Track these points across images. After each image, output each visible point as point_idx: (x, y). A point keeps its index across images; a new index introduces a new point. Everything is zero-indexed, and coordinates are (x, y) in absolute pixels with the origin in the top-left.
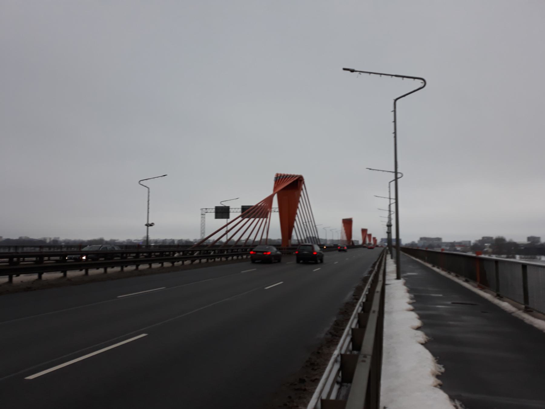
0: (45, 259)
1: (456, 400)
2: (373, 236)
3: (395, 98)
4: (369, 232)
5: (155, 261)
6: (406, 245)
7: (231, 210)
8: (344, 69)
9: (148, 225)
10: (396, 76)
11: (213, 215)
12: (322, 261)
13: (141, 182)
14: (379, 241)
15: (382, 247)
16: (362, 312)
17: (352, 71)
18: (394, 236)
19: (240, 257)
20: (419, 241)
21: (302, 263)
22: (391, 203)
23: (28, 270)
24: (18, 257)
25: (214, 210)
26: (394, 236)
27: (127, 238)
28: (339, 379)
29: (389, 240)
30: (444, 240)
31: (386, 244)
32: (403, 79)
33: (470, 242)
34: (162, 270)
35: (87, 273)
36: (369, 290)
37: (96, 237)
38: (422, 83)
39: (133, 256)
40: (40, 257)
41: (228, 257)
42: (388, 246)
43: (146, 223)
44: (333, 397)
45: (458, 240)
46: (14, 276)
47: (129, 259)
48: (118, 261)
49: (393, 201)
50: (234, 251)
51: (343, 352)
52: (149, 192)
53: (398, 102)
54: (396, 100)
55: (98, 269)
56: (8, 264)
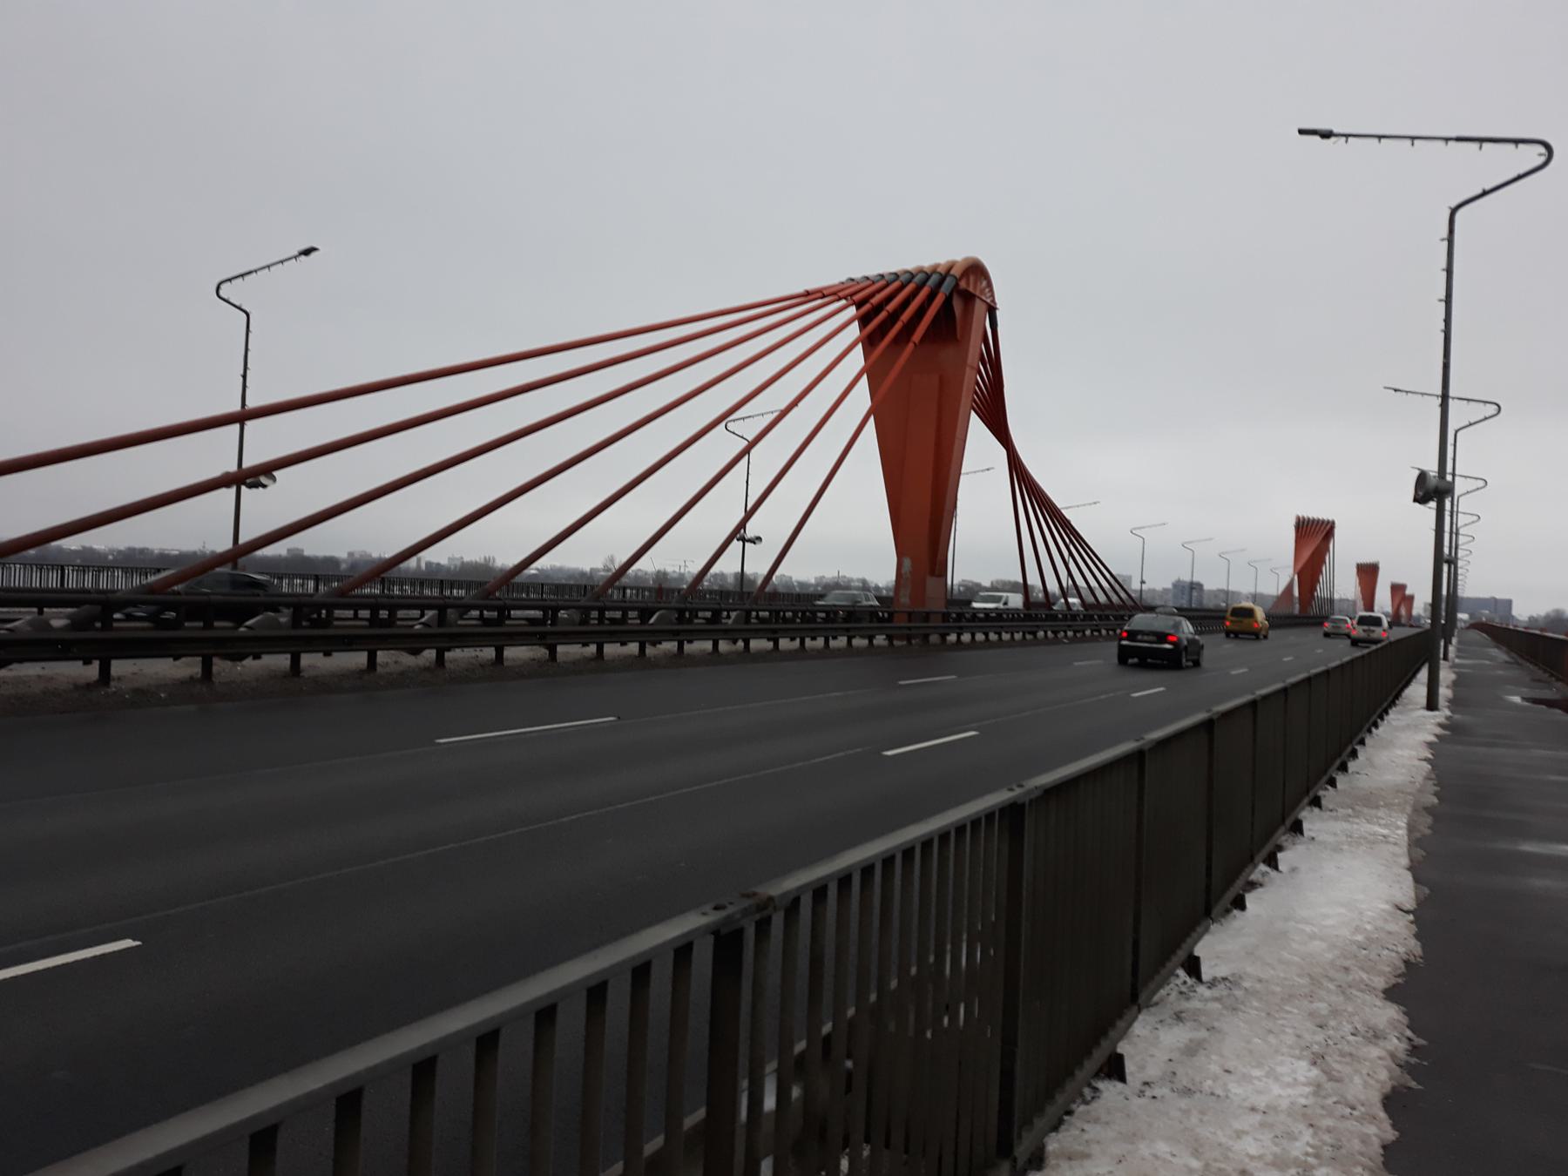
0: (399, 616)
3: (1454, 204)
4: (1408, 592)
5: (758, 634)
8: (1301, 132)
10: (1459, 139)
12: (1197, 664)
17: (1326, 135)
19: (966, 637)
21: (1133, 665)
23: (348, 643)
24: (393, 609)
27: (819, 574)
34: (826, 652)
35: (440, 658)
38: (1540, 155)
39: (704, 618)
40: (551, 611)
41: (948, 634)
47: (631, 624)
48: (636, 628)
54: (1454, 212)
55: (623, 644)
56: (146, 624)
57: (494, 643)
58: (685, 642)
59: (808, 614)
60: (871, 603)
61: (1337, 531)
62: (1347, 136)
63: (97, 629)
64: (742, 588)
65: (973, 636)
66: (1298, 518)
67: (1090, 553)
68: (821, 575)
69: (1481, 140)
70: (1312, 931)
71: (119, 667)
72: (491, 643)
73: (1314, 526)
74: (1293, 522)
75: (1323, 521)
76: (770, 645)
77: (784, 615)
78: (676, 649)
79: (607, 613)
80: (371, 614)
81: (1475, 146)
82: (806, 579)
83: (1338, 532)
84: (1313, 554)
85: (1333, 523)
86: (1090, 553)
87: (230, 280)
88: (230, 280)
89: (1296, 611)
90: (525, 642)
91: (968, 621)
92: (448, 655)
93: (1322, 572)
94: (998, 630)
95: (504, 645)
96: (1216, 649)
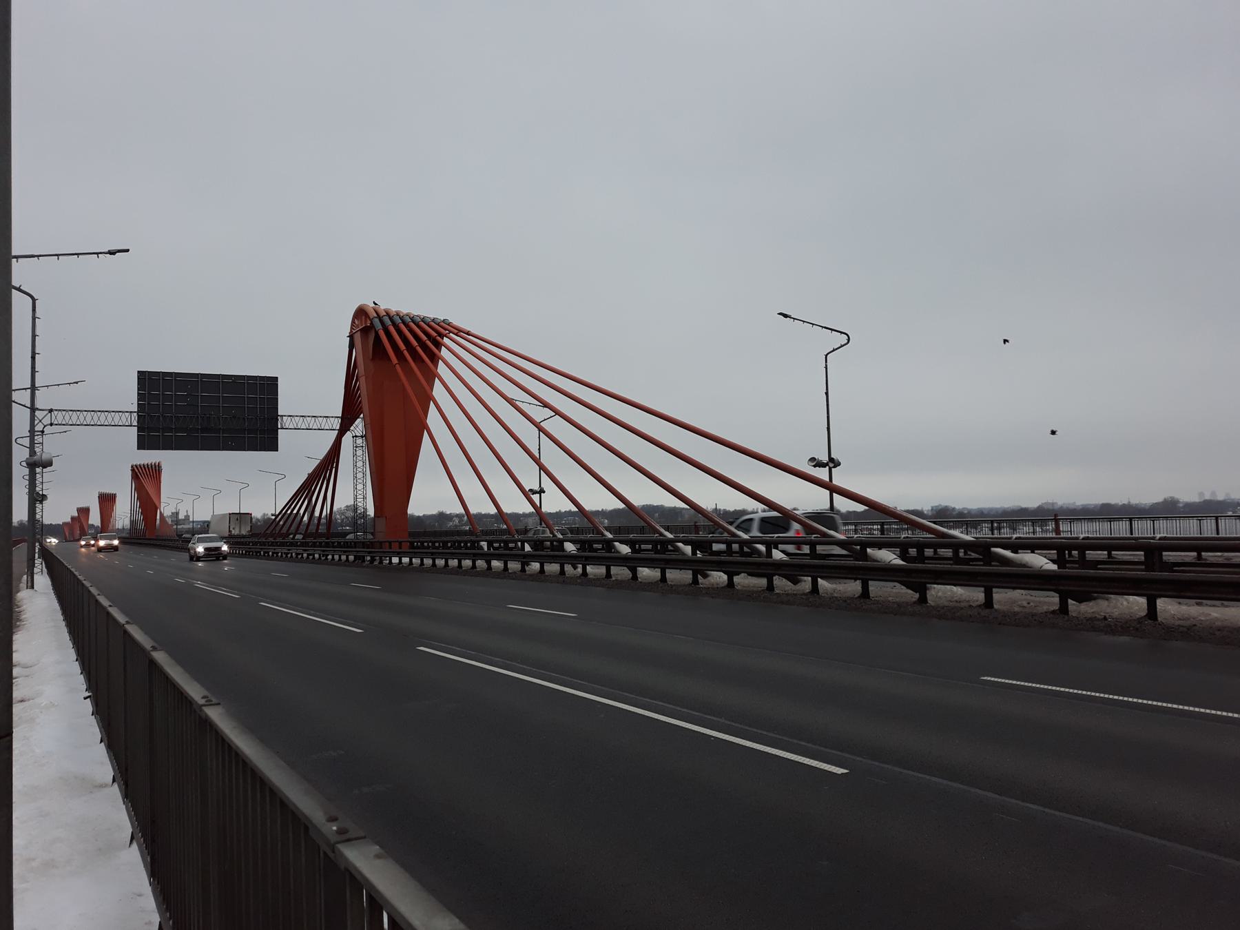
57: (693, 568)
59: (555, 543)
60: (1214, 536)
63: (450, 541)
65: (422, 563)
67: (300, 503)
70: (39, 558)
71: (1000, 596)
72: (808, 574)
76: (914, 596)
77: (640, 547)
78: (457, 564)
79: (963, 550)
80: (917, 551)
82: (1072, 502)
86: (300, 503)
87: (842, 346)
88: (842, 346)
92: (736, 579)
95: (564, 563)
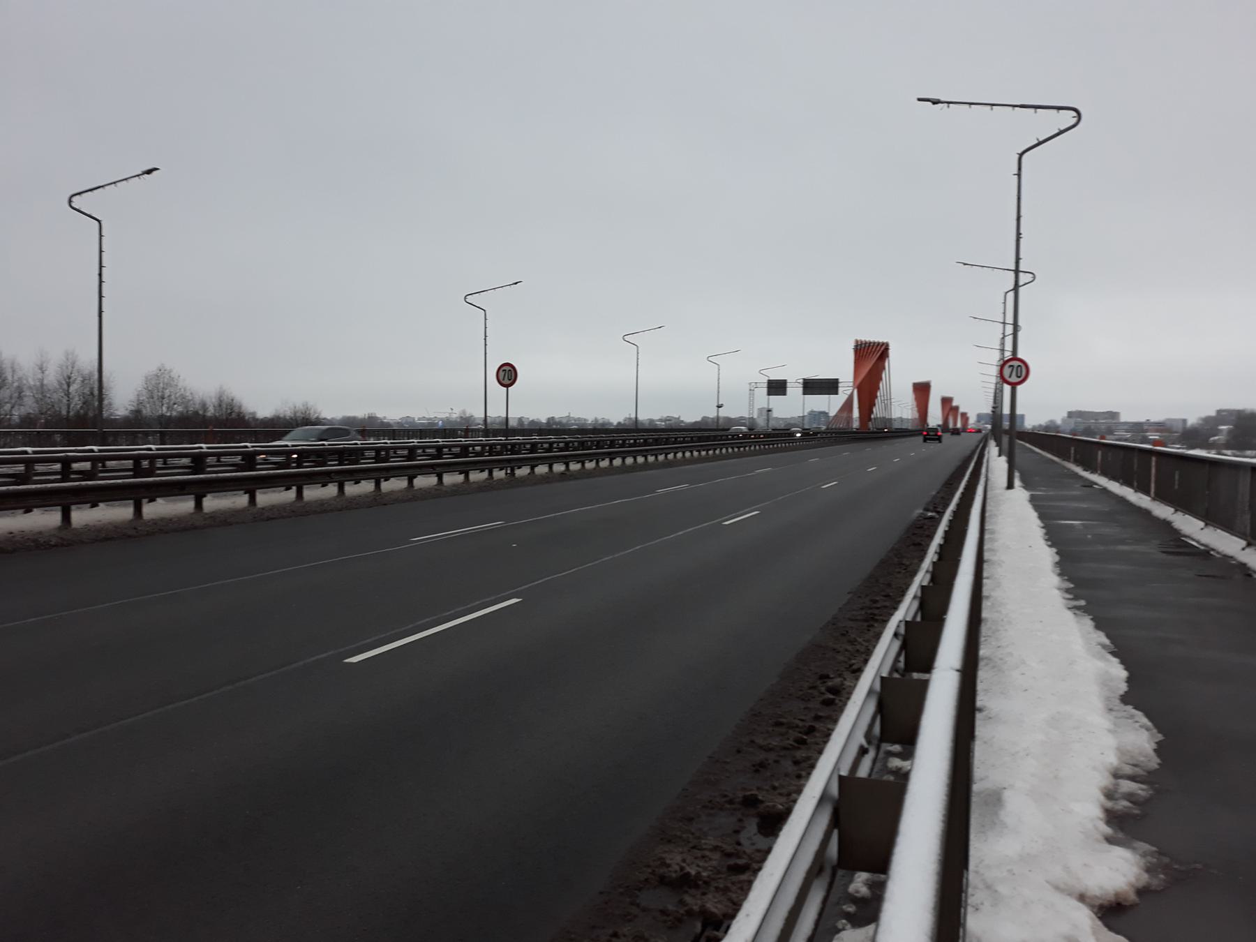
1: (1145, 774)
2: (961, 410)
4: (954, 404)
6: (1034, 428)
7: (788, 385)
8: (919, 100)
9: (719, 407)
11: (765, 390)
13: (469, 299)
14: (972, 420)
15: (979, 431)
16: (931, 584)
17: (935, 102)
18: (1006, 410)
20: (1063, 420)
22: (1006, 334)
25: (766, 385)
26: (1006, 410)
28: (902, 665)
29: (996, 416)
30: (1125, 417)
31: (989, 427)
32: (1036, 112)
33: (1184, 421)
36: (976, 463)
37: (359, 411)
42: (993, 430)
43: (716, 404)
44: (863, 772)
45: (1156, 417)
46: (587, 461)
49: (1009, 329)
50: (627, 442)
51: (909, 619)
52: (719, 370)
53: (1025, 157)
54: (1021, 155)
57: (285, 484)
58: (382, 480)
61: (891, 352)
62: (949, 103)
64: (768, 424)
66: (857, 341)
68: (551, 416)
69: (1040, 143)
73: (871, 348)
74: (852, 345)
75: (879, 343)
81: (1032, 110)
83: (892, 352)
84: (870, 370)
85: (887, 345)
89: (856, 424)
90: (280, 484)
91: (561, 450)
93: (879, 388)
94: (645, 454)
96: (946, 437)
